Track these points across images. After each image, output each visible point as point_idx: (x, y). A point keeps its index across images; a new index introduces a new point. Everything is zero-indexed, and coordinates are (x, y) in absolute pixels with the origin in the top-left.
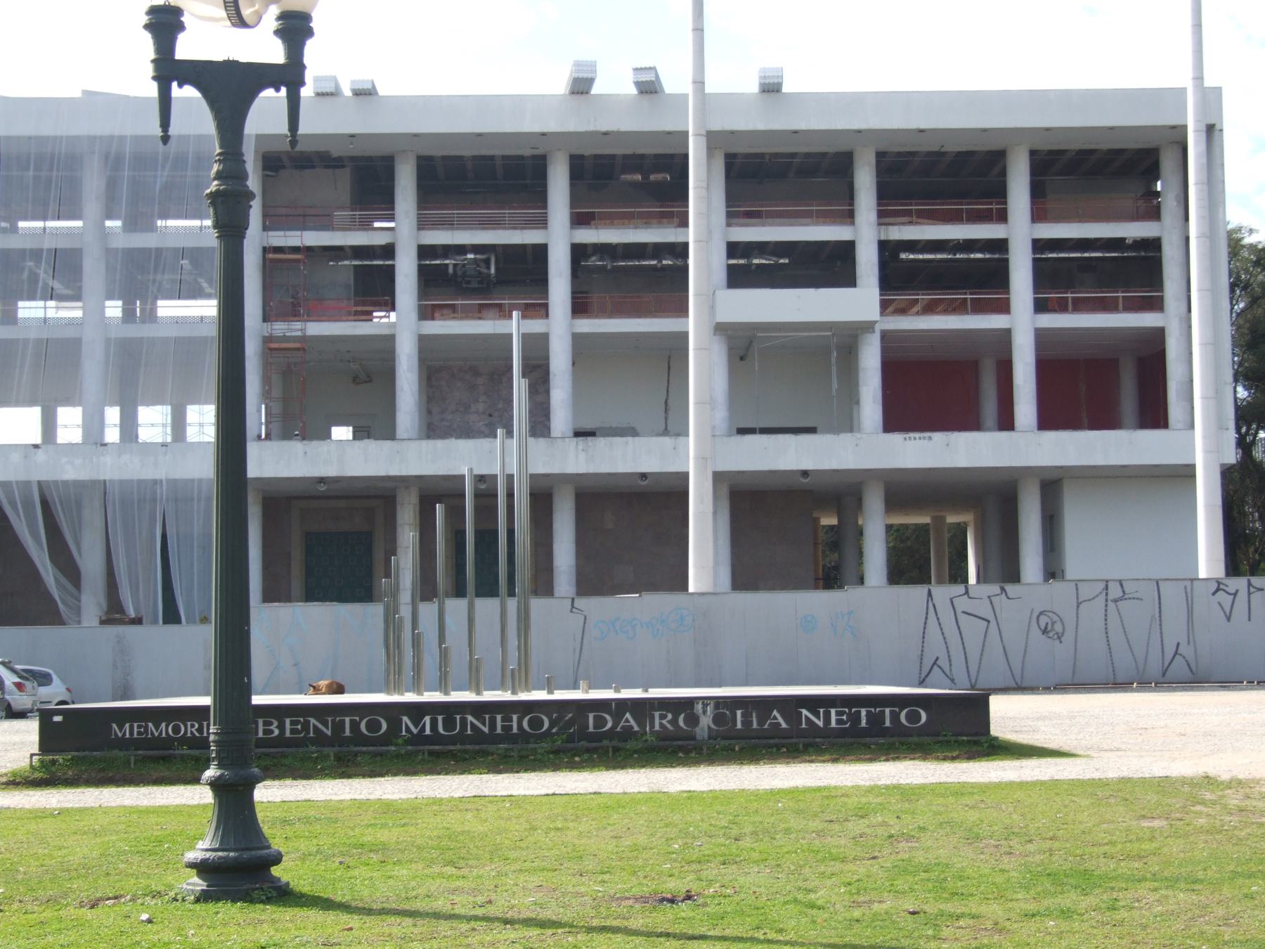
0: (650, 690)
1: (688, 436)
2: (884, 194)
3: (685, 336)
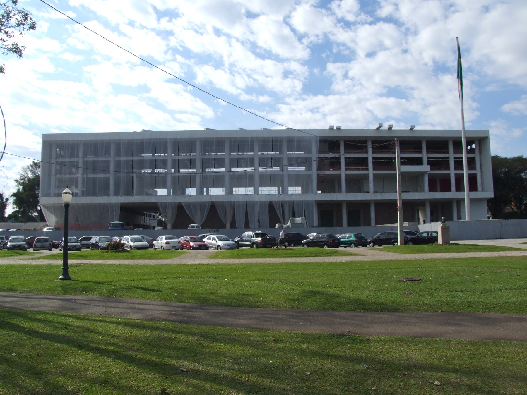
0: (53, 250)
1: (464, 191)
2: (428, 149)
3: (463, 174)
